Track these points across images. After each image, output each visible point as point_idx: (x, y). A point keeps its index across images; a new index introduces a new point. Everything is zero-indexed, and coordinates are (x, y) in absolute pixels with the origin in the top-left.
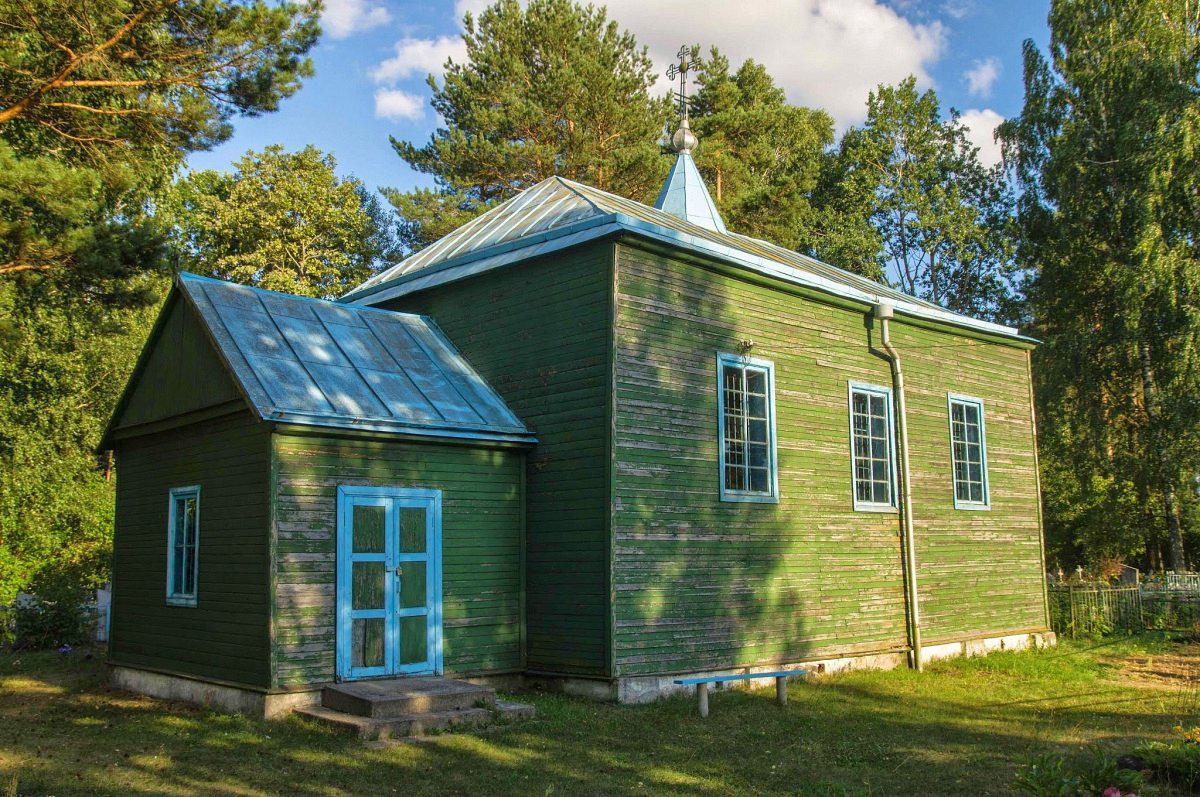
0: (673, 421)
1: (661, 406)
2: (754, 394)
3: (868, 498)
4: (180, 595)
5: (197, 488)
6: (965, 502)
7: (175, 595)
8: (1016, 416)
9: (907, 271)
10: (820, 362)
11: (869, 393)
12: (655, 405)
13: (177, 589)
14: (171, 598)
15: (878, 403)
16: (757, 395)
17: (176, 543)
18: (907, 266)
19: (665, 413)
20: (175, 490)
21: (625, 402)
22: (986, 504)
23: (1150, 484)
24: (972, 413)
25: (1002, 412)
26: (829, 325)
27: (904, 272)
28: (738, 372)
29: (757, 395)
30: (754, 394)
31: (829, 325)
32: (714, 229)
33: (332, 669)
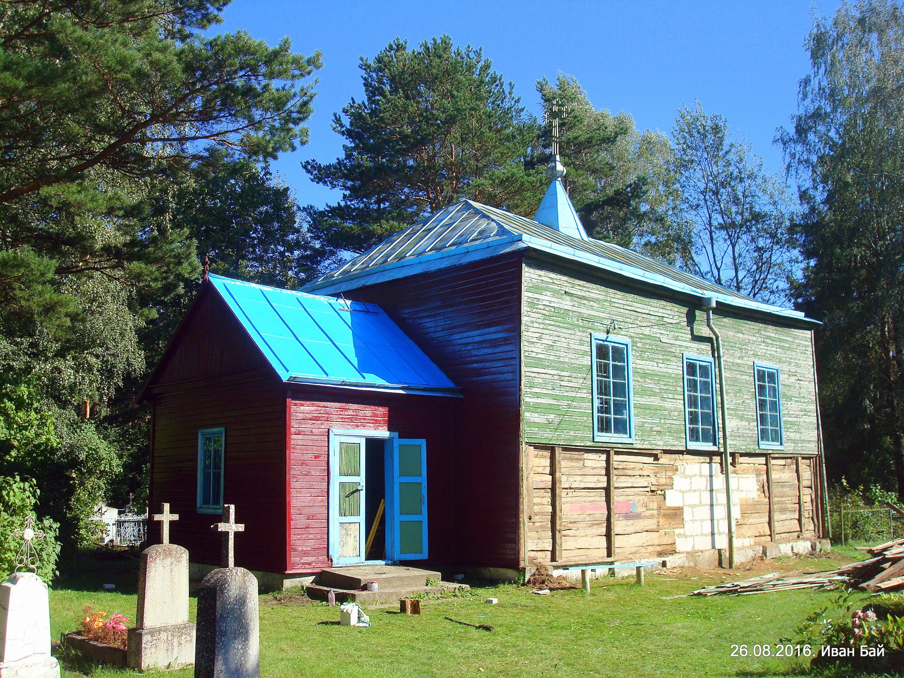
0: (563, 383)
1: (555, 372)
2: (616, 363)
3: (697, 440)
4: (209, 506)
5: (222, 429)
6: (767, 443)
7: (203, 506)
8: (803, 379)
9: (715, 261)
10: (663, 340)
11: (698, 362)
12: (550, 372)
13: (206, 501)
14: (201, 508)
15: (705, 371)
16: (619, 364)
17: (204, 469)
18: (714, 256)
19: (556, 377)
20: (203, 431)
21: (529, 369)
22: (630, 437)
23: (390, 160)
24: (772, 377)
25: (793, 375)
26: (669, 312)
27: (712, 260)
28: (606, 347)
29: (619, 364)
30: (616, 363)
31: (669, 312)
32: (578, 237)
33: (775, 476)
